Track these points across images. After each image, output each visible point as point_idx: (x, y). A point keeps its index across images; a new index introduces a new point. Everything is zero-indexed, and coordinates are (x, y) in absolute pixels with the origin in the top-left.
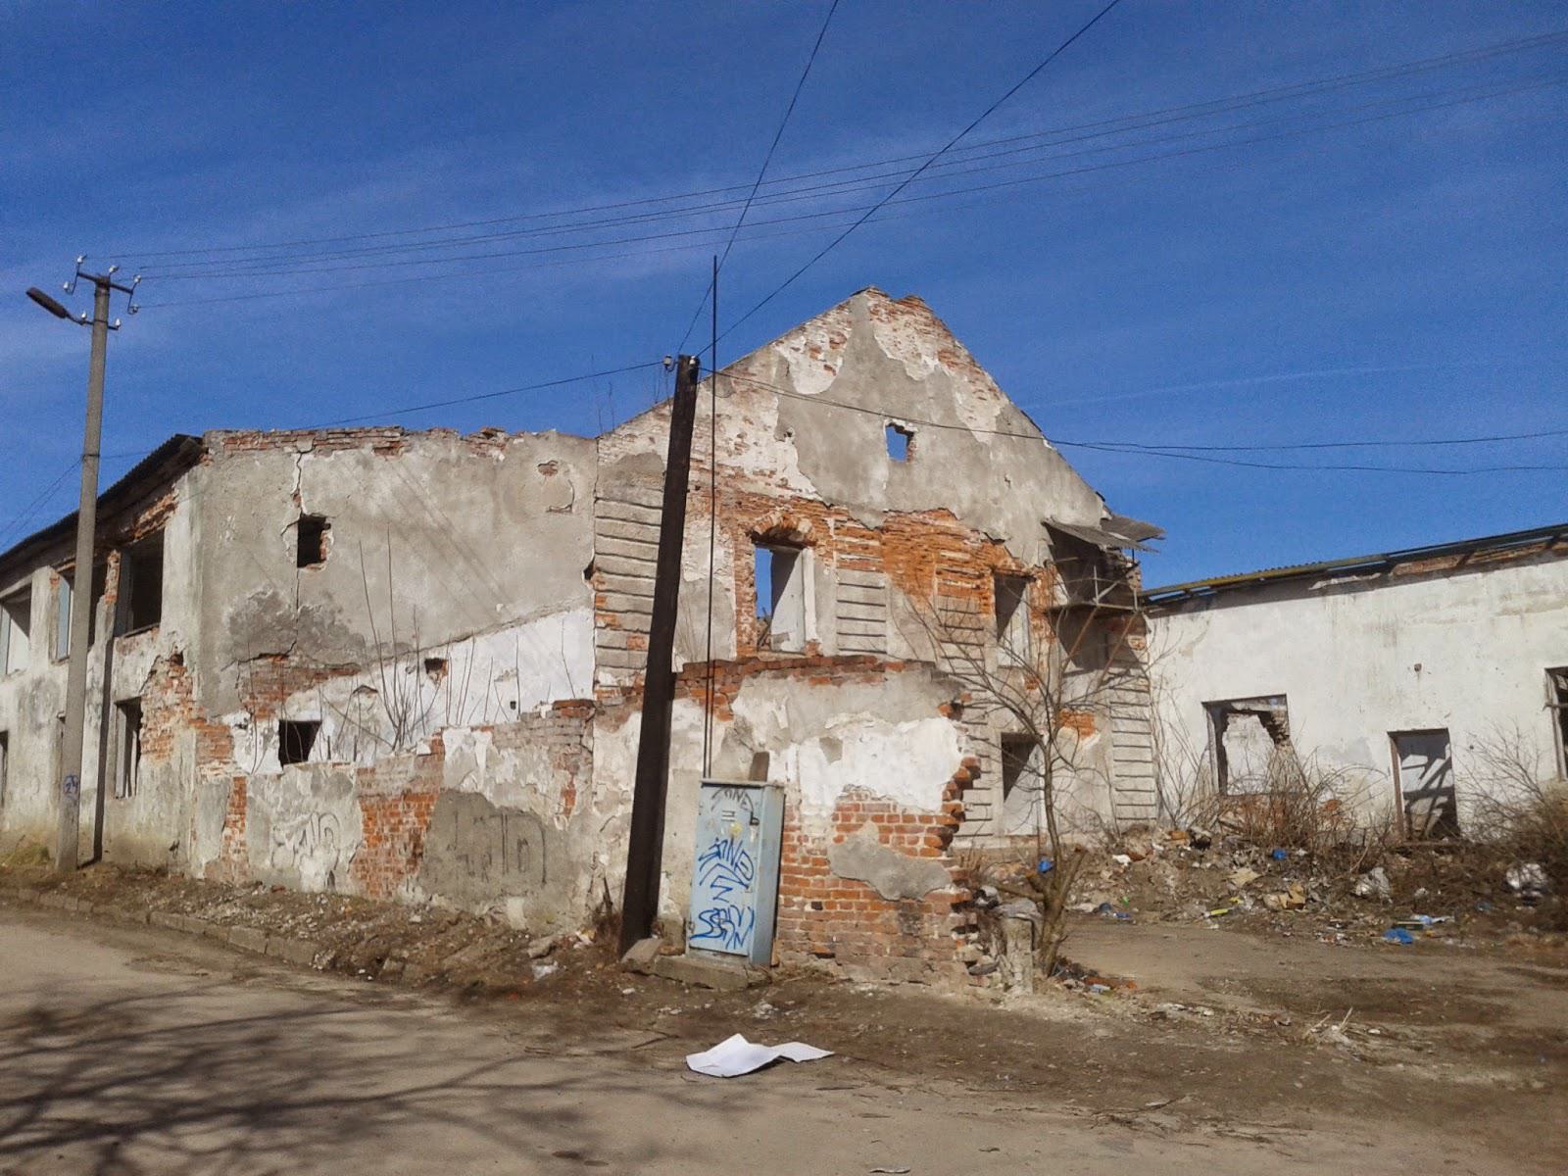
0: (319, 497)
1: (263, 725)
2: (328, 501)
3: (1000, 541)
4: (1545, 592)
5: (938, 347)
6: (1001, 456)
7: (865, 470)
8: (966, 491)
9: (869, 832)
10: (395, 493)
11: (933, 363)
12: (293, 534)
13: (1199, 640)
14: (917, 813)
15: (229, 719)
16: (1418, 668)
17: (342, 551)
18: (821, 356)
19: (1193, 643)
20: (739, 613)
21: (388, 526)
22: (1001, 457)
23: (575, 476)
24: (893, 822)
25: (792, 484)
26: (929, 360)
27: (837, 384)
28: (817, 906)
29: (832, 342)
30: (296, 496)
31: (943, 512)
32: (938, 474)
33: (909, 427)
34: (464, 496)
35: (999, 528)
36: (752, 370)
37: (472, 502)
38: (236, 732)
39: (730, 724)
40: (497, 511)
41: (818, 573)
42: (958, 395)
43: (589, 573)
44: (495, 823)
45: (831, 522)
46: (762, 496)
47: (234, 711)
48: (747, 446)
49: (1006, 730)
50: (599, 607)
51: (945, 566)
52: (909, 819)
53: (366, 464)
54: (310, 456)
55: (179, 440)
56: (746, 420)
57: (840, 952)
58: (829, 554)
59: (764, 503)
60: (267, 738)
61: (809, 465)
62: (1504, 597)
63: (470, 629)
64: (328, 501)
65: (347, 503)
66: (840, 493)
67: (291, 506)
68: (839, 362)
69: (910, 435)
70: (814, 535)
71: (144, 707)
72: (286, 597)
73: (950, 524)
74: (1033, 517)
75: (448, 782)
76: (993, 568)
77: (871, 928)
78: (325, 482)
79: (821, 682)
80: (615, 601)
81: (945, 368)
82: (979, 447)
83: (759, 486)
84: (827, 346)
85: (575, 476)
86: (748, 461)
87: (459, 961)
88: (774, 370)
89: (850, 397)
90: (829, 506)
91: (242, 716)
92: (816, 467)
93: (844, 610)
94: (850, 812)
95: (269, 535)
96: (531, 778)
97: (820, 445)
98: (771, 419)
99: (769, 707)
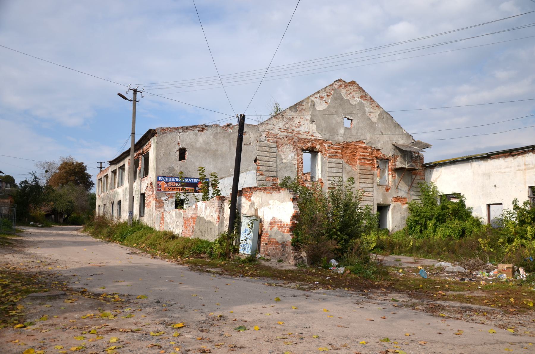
0: (184, 143)
1: (171, 200)
2: (187, 144)
3: (379, 150)
4: (529, 164)
5: (360, 95)
6: (380, 125)
7: (337, 130)
8: (368, 137)
9: (276, 228)
10: (204, 141)
11: (359, 100)
12: (178, 153)
13: (438, 177)
14: (285, 223)
15: (163, 198)
16: (495, 186)
17: (190, 157)
18: (324, 99)
19: (437, 178)
20: (298, 171)
21: (200, 150)
22: (380, 126)
23: (252, 135)
24: (281, 225)
25: (314, 135)
26: (357, 99)
27: (329, 107)
28: (266, 244)
29: (327, 95)
30: (178, 143)
31: (361, 142)
32: (360, 131)
33: (351, 118)
34: (221, 142)
35: (379, 146)
36: (303, 104)
37: (223, 143)
38: (164, 202)
39: (250, 202)
40: (230, 145)
41: (322, 160)
42: (366, 108)
43: (255, 161)
44: (206, 224)
45: (326, 145)
46: (305, 139)
47: (164, 196)
48: (301, 125)
49: (379, 203)
50: (257, 171)
51: (361, 157)
52: (284, 225)
53: (196, 135)
54: (182, 133)
55: (150, 130)
56: (301, 118)
57: (271, 254)
58: (325, 154)
59: (306, 141)
60: (172, 203)
61: (319, 130)
62: (518, 166)
63: (223, 176)
64: (187, 144)
65: (192, 145)
66: (329, 138)
67: (177, 146)
68: (330, 101)
69: (352, 120)
70: (321, 149)
71: (146, 195)
72: (177, 169)
73: (364, 145)
74: (390, 142)
75: (198, 215)
76: (376, 157)
77: (276, 249)
78: (186, 140)
79: (268, 193)
80: (262, 168)
81: (363, 101)
82: (373, 123)
83: (305, 136)
84: (326, 97)
85: (252, 135)
86: (302, 129)
87: (497, 280)
88: (310, 104)
89: (333, 110)
90: (326, 141)
91: (166, 198)
92: (322, 130)
93: (330, 170)
94: (272, 224)
95: (172, 153)
96: (212, 214)
97: (323, 124)
98: (309, 118)
99: (258, 198)
